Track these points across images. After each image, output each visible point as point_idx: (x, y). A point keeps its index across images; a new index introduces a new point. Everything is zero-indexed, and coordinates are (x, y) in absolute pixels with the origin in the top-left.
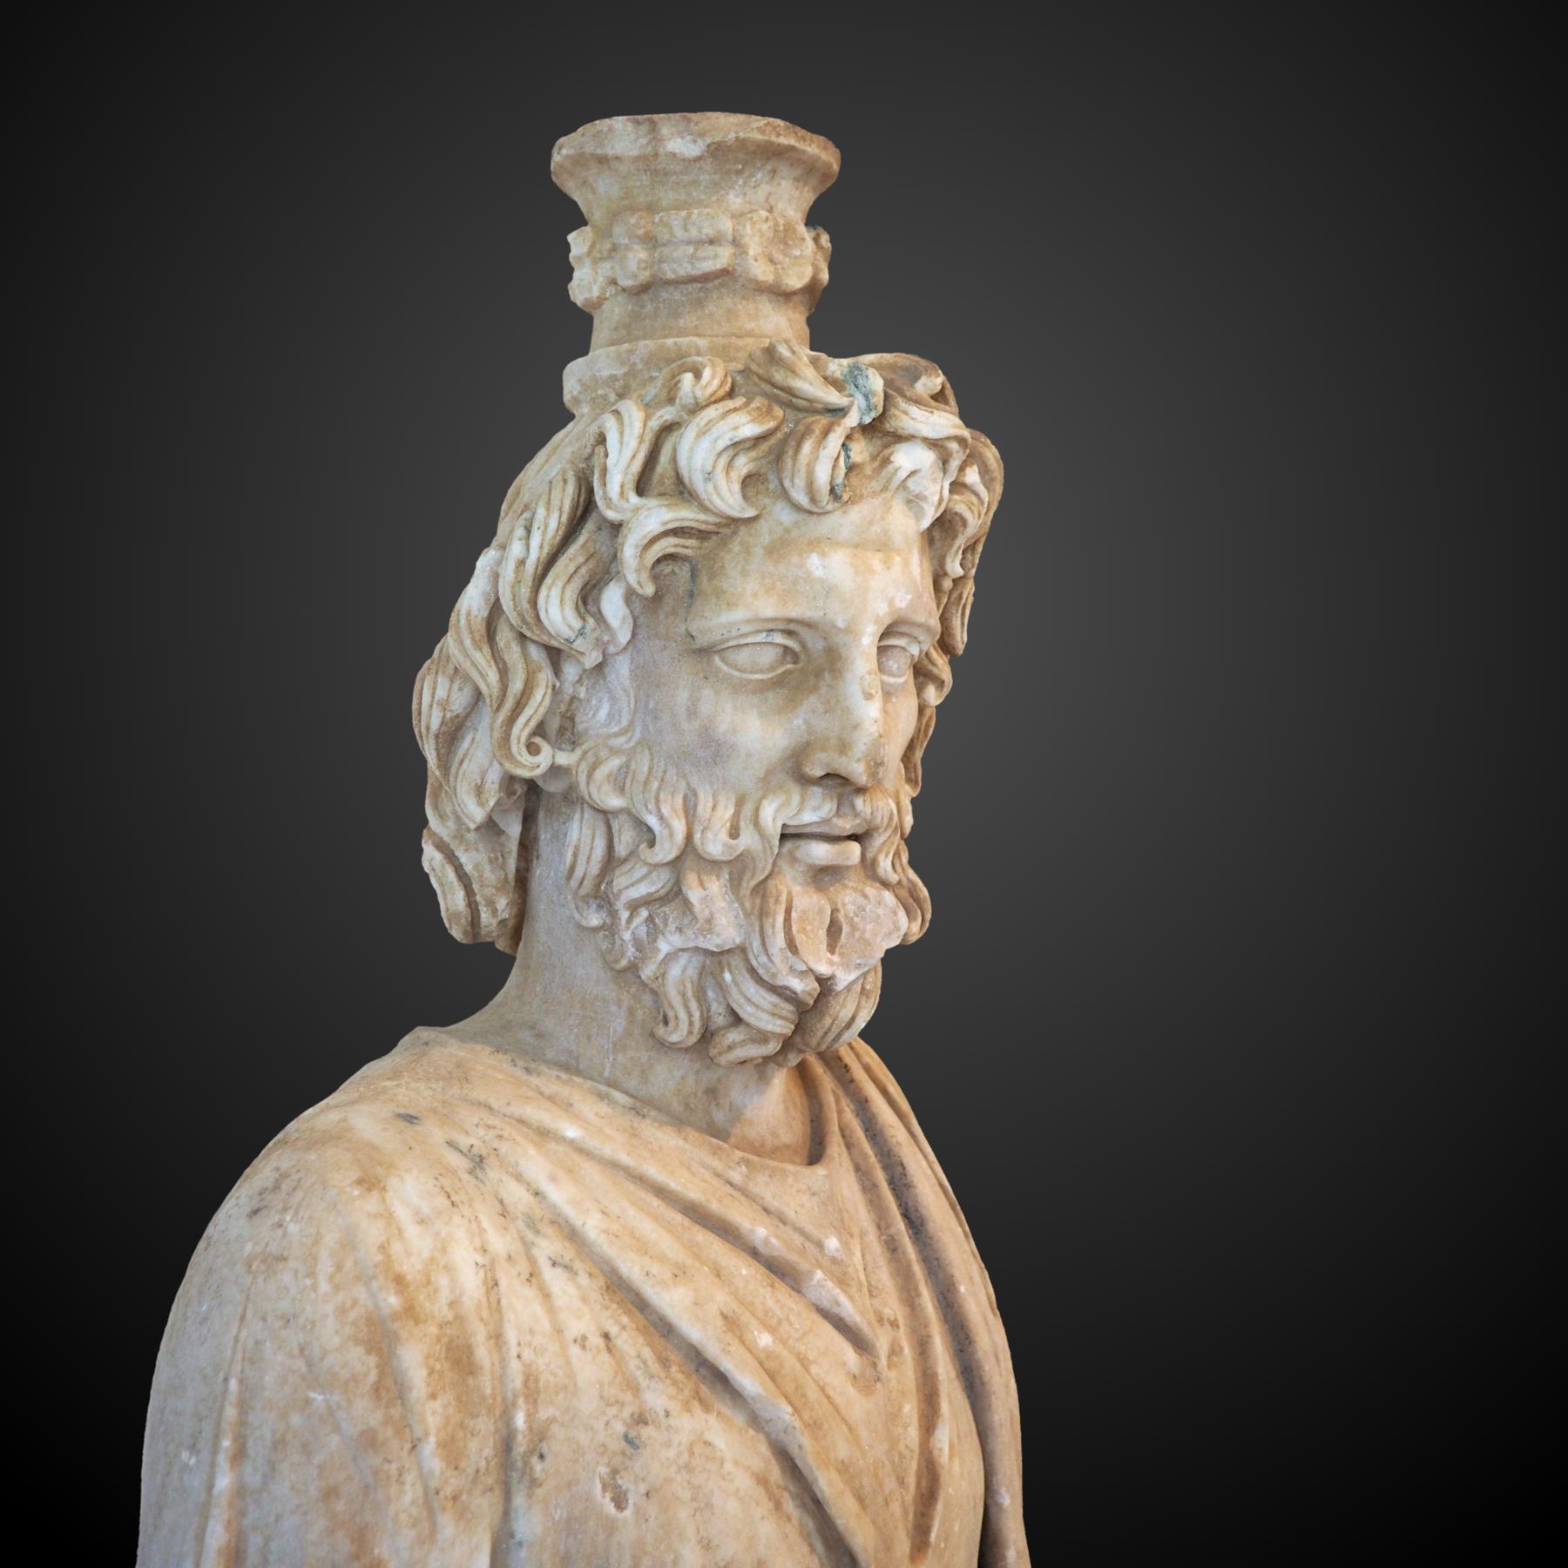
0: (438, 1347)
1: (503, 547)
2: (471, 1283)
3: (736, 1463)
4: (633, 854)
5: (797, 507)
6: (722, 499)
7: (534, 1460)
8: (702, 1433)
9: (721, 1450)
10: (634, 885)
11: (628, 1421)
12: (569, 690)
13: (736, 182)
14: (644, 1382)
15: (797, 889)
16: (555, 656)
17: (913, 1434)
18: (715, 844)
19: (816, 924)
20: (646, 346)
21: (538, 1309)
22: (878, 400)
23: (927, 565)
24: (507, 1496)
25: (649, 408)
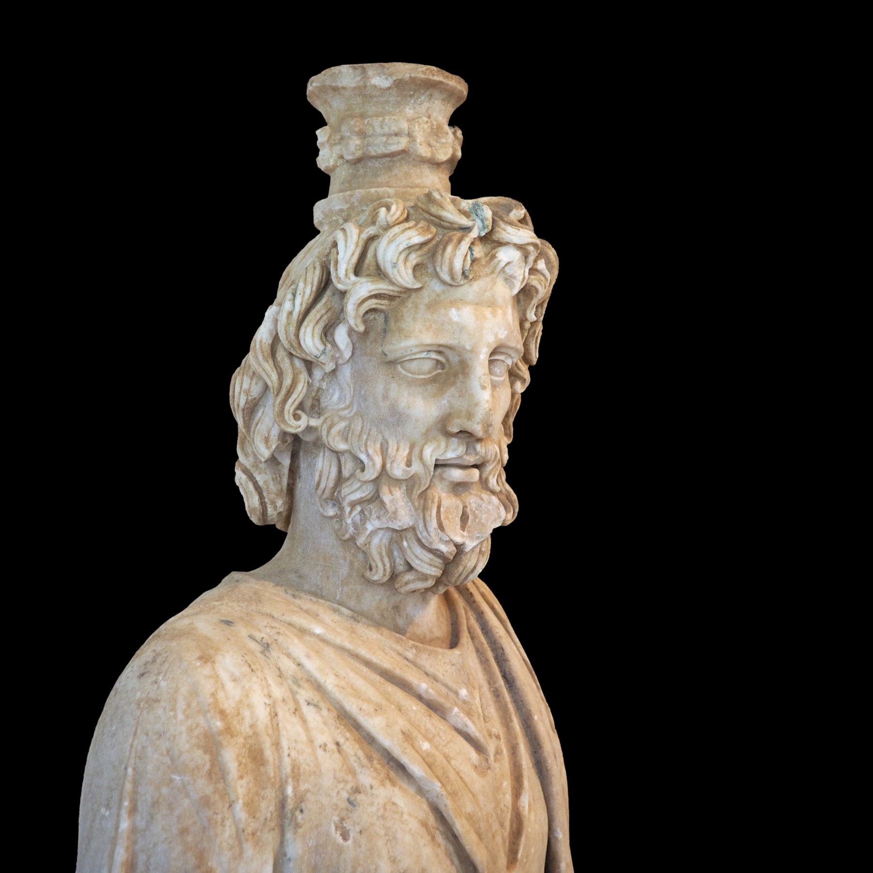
0: (244, 750)
1: (280, 305)
2: (262, 714)
3: (410, 815)
4: (352, 475)
5: (444, 282)
6: (402, 278)
7: (298, 813)
8: (391, 798)
9: (401, 807)
10: (353, 493)
11: (350, 791)
12: (317, 384)
13: (410, 101)
14: (358, 770)
15: (444, 495)
16: (309, 365)
17: (508, 798)
18: (398, 470)
19: (454, 514)
20: (359, 193)
21: (299, 729)
22: (489, 223)
23: (516, 315)
24: (282, 833)
25: (361, 227)
